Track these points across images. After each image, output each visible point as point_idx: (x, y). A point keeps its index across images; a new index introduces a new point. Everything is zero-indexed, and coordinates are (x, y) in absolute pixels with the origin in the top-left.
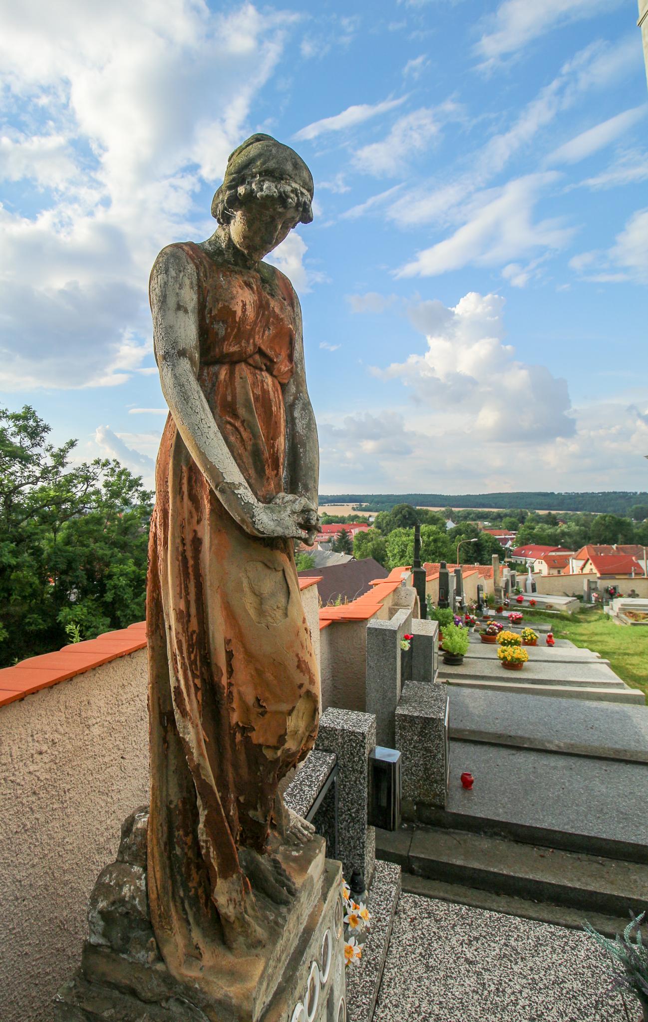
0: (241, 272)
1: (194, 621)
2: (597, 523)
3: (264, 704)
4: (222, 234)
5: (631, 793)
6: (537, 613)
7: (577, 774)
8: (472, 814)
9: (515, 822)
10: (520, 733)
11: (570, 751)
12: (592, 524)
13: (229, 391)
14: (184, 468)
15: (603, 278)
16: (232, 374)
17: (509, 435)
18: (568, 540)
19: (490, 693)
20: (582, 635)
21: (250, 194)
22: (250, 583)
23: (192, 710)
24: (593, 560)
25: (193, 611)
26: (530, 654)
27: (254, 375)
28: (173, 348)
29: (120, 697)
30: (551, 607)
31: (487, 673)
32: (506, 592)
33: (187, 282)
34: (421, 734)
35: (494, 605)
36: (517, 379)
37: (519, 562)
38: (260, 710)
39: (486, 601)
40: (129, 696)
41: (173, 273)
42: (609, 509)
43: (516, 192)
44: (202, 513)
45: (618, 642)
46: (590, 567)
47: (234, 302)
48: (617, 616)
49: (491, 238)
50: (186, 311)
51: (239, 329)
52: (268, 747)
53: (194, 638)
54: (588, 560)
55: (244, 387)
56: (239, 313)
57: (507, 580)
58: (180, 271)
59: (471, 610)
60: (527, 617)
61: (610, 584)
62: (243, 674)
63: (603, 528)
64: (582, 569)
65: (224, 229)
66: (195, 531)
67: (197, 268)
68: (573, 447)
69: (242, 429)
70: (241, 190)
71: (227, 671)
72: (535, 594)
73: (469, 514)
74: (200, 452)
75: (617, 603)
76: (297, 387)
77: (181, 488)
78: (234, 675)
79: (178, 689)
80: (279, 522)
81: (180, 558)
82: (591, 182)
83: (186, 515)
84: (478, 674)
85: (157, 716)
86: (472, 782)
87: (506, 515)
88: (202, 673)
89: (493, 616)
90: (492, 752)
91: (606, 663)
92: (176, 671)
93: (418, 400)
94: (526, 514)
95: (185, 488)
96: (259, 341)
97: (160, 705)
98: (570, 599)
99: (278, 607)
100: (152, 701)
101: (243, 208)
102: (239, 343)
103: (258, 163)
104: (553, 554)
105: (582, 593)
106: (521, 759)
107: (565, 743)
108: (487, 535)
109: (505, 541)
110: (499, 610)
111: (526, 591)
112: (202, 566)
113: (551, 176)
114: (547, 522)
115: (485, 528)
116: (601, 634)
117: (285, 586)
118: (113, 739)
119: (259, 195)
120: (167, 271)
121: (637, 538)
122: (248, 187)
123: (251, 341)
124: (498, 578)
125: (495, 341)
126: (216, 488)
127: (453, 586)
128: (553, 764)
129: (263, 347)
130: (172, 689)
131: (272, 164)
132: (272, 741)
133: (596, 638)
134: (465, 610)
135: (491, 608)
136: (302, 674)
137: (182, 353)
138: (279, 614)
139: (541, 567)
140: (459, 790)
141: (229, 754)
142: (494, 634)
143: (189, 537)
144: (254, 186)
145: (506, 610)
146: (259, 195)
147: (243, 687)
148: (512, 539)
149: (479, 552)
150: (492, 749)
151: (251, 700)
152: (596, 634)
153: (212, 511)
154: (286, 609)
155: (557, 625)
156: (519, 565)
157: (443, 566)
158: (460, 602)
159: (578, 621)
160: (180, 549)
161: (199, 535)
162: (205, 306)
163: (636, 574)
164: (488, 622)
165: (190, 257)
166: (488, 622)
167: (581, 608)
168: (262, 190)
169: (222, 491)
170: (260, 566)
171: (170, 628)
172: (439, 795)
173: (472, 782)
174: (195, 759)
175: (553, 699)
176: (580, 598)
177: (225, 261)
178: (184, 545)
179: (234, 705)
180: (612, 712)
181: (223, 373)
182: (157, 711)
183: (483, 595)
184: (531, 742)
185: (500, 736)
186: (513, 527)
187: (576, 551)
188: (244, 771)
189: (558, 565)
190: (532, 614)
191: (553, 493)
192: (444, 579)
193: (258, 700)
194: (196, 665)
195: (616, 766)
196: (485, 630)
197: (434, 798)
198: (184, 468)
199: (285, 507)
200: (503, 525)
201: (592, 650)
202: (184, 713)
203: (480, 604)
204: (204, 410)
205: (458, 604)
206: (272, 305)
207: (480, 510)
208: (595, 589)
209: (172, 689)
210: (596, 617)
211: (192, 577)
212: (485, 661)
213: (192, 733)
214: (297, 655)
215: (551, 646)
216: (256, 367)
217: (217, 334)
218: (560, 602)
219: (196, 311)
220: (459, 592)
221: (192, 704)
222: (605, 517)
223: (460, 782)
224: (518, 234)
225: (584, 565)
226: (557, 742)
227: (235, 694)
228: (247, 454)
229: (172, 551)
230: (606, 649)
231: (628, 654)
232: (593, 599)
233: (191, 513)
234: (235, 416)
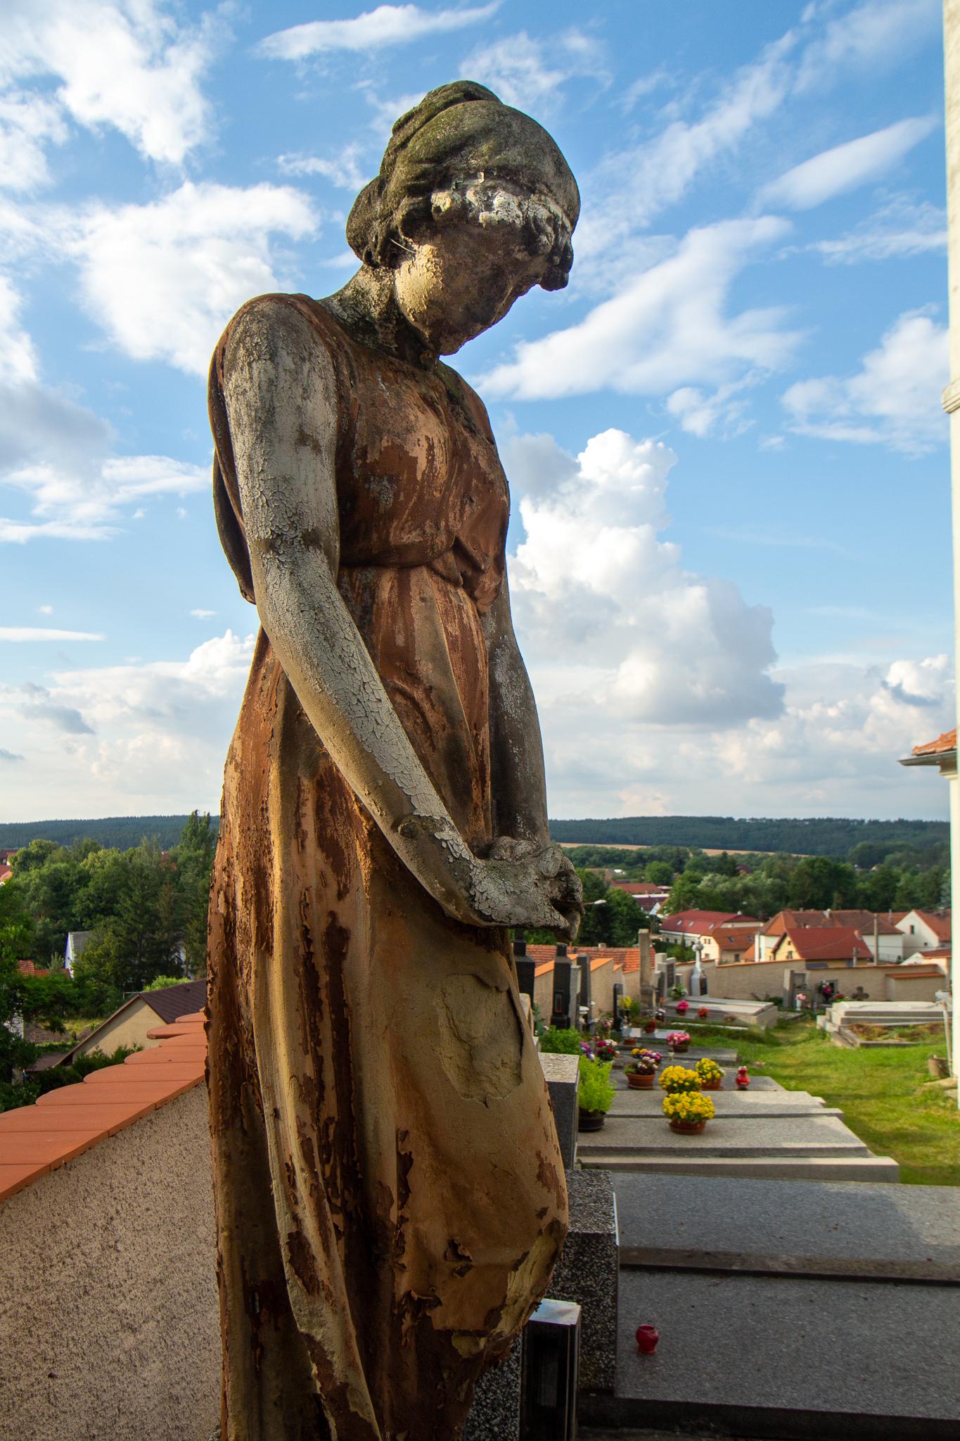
0: (413, 375)
1: (331, 1097)
2: (800, 874)
3: (467, 1254)
4: (374, 288)
5: (909, 1333)
6: (712, 1031)
7: (822, 1310)
8: (660, 1397)
9: (734, 1403)
10: (722, 1246)
11: (807, 1270)
12: (792, 874)
13: (400, 624)
14: (306, 783)
15: (839, 433)
16: (403, 588)
17: (677, 712)
18: (753, 900)
19: (666, 1178)
20: (785, 1066)
21: (462, 213)
22: (450, 1019)
23: (332, 1278)
24: (792, 937)
25: (329, 1077)
26: (716, 1104)
27: (446, 594)
28: (293, 526)
29: (47, 1252)
31: (645, 1143)
32: (659, 995)
33: (319, 385)
34: (574, 1265)
35: (638, 1018)
36: (687, 604)
37: (672, 941)
38: (458, 1265)
39: (627, 1013)
40: (63, 1247)
41: (287, 361)
42: (820, 848)
43: (705, 249)
44: (348, 876)
45: (844, 1078)
46: (788, 948)
47: (412, 438)
48: (839, 1033)
49: (652, 335)
50: (317, 448)
51: (421, 497)
52: (464, 1333)
53: (331, 1132)
54: (784, 936)
55: (429, 619)
56: (422, 464)
57: (662, 974)
58: (303, 359)
59: (604, 1029)
60: (695, 1039)
61: (823, 977)
62: (428, 1195)
63: (808, 881)
64: (775, 951)
65: (379, 279)
66: (332, 914)
67: (333, 356)
68: (771, 737)
69: (426, 706)
70: (442, 200)
71: (399, 1194)
72: (705, 998)
73: (589, 854)
74: (362, 751)
75: (839, 1010)
76: (499, 622)
77: (299, 824)
78: (410, 1200)
79: (297, 1240)
80: (518, 897)
81: (301, 970)
82: (825, 246)
83: (313, 881)
84: (631, 1145)
85: (240, 1294)
86: (655, 1341)
87: (652, 857)
88: (344, 1202)
89: (639, 1040)
90: (682, 1284)
91: (838, 1115)
92: (292, 1200)
93: (641, 654)
94: (687, 854)
95: (309, 824)
96: (456, 526)
97: (244, 1273)
98: (763, 1005)
99: (503, 1063)
100: (231, 1266)
101: (438, 239)
102: (420, 526)
103: (484, 148)
104: (729, 926)
105: (781, 995)
106: (728, 1290)
107: (797, 1258)
108: (619, 892)
109: (650, 903)
110: (649, 1028)
111: (691, 994)
112: (348, 985)
113: (767, 228)
114: (719, 870)
115: (617, 879)
116: (816, 1064)
117: (512, 1020)
118: (34, 1340)
119: (483, 216)
120: (273, 356)
121: (861, 899)
122: (457, 196)
123: (443, 524)
124: (647, 970)
125: (644, 530)
126: (394, 827)
127: (576, 988)
128: (781, 1296)
129: (463, 539)
130: (283, 1240)
131: (513, 156)
132: (473, 1321)
133: (810, 1071)
134: (593, 1028)
135: (636, 1025)
136: (545, 1190)
137: (311, 539)
138: (505, 1076)
139: (712, 949)
140: (634, 1356)
141: (386, 1357)
142: (651, 1071)
143: (319, 928)
144: (470, 196)
145: (660, 1027)
146: (483, 216)
147: (425, 1221)
148: (661, 900)
149: (613, 925)
150: (679, 1278)
151: (438, 1246)
152: (808, 1065)
153: (375, 873)
154: (519, 1065)
155: (751, 1053)
156: (672, 946)
157: (561, 952)
158: (585, 1017)
159: (775, 1043)
160: (302, 951)
161: (343, 921)
162: (352, 443)
163: (859, 959)
164: (635, 1051)
165: (317, 329)
166: (635, 1051)
167: (779, 1021)
168: (489, 207)
169: (409, 834)
170: (469, 983)
171: (276, 1114)
172: (604, 1371)
173: (655, 1341)
174: (337, 1374)
175: (770, 1183)
176: (778, 1002)
177: (380, 346)
178: (309, 942)
179: (405, 1260)
180: (864, 1199)
181: (386, 587)
182: (240, 1286)
183: (626, 1000)
184: (744, 1261)
185: (692, 1254)
186: (664, 879)
187: (765, 920)
188: (411, 1385)
189: (736, 945)
190: (703, 1033)
191: (730, 819)
192: (562, 973)
193: (453, 1245)
194: (335, 1184)
195: (880, 1290)
196: (635, 1066)
197: (595, 1376)
198: (306, 783)
199: (524, 866)
200: (647, 875)
201: (814, 1094)
202: (312, 1286)
203: (619, 1015)
204: (366, 665)
205: (582, 1020)
206: (473, 452)
207: (608, 847)
208: (801, 988)
209: (283, 1240)
210: (805, 1035)
211: (326, 1008)
212: (641, 1122)
213: (326, 1324)
214: (538, 1155)
215: (743, 1089)
216: (447, 579)
217: (376, 502)
218: (746, 1010)
219: (334, 450)
220: (584, 999)
221: (330, 1266)
222: (814, 862)
223: (634, 1342)
224: (701, 336)
226: (784, 1257)
227: (409, 1238)
228: (436, 756)
229: (285, 956)
230: (827, 1089)
231: (860, 1097)
232: (799, 1003)
233: (322, 875)
234: (414, 678)
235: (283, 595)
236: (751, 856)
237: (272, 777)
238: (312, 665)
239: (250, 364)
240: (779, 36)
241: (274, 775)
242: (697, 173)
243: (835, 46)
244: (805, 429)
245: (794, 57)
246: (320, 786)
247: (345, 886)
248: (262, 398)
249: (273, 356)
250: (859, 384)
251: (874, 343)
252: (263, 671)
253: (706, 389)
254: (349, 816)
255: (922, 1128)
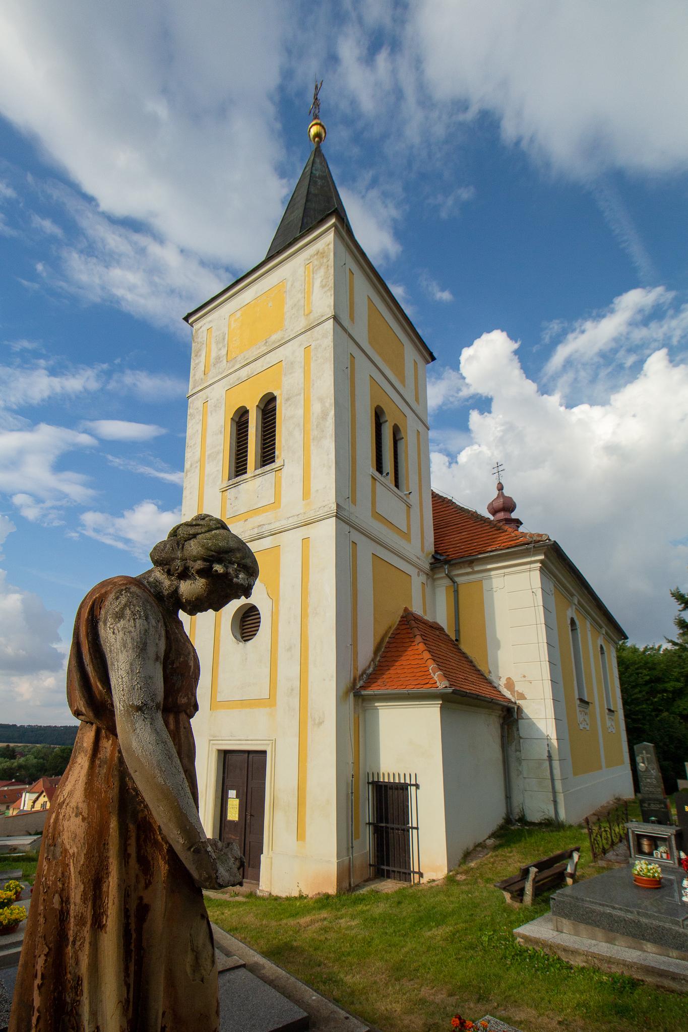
14: (131, 827)
15: (109, 541)
18: (23, 772)
30: (15, 849)
44: (152, 875)
66: (141, 898)
70: (219, 568)
77: (126, 850)
82: (110, 457)
95: (132, 850)
98: (35, 837)
104: (6, 788)
168: (237, 577)
187: (30, 784)
198: (131, 827)
199: (226, 854)
225: (37, 798)
233: (137, 876)
235: (146, 735)
236: (24, 747)
237: (112, 826)
238: (161, 770)
239: (134, 619)
240: (104, 363)
241: (113, 824)
242: (49, 397)
243: (129, 378)
244: (90, 533)
245: (109, 374)
246: (139, 828)
247: (150, 881)
248: (141, 638)
249: (147, 618)
250: (120, 522)
251: (131, 508)
252: (98, 762)
253: (38, 500)
254: (156, 843)
255: (108, 892)
